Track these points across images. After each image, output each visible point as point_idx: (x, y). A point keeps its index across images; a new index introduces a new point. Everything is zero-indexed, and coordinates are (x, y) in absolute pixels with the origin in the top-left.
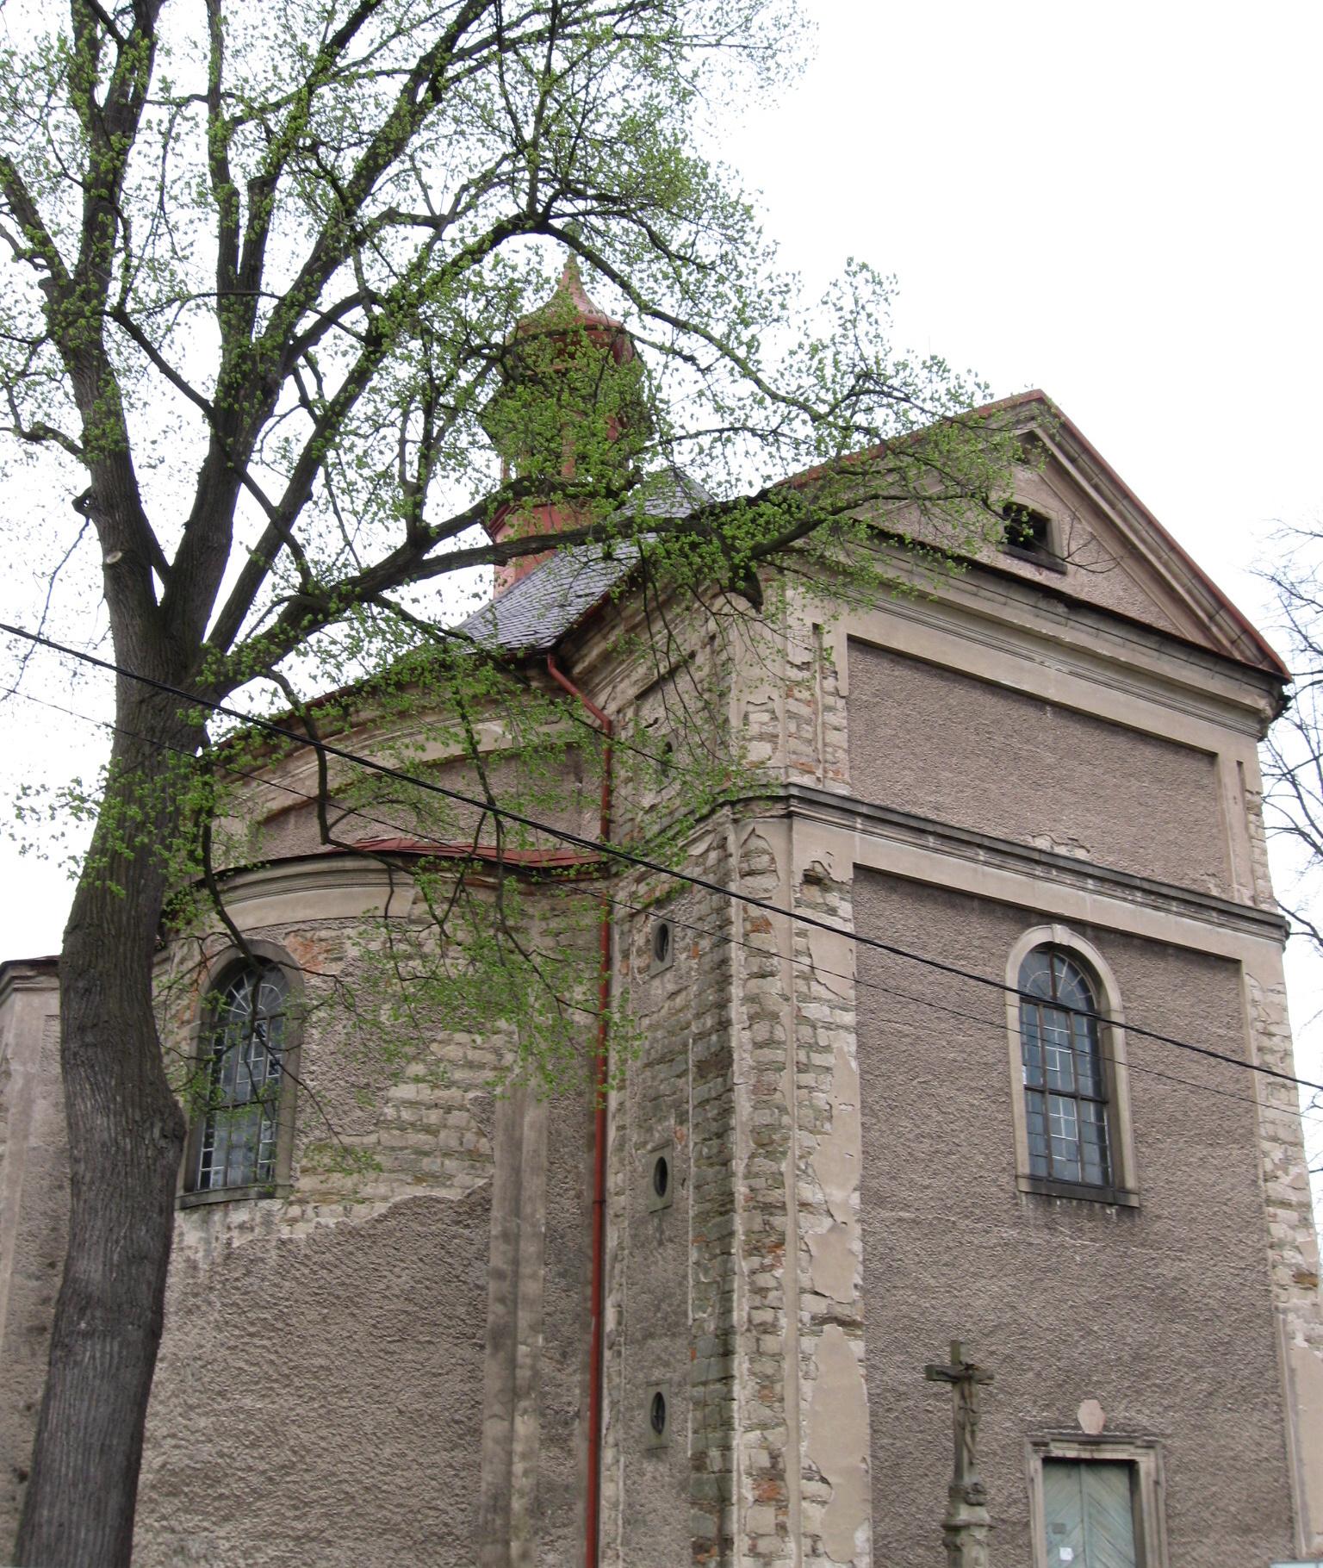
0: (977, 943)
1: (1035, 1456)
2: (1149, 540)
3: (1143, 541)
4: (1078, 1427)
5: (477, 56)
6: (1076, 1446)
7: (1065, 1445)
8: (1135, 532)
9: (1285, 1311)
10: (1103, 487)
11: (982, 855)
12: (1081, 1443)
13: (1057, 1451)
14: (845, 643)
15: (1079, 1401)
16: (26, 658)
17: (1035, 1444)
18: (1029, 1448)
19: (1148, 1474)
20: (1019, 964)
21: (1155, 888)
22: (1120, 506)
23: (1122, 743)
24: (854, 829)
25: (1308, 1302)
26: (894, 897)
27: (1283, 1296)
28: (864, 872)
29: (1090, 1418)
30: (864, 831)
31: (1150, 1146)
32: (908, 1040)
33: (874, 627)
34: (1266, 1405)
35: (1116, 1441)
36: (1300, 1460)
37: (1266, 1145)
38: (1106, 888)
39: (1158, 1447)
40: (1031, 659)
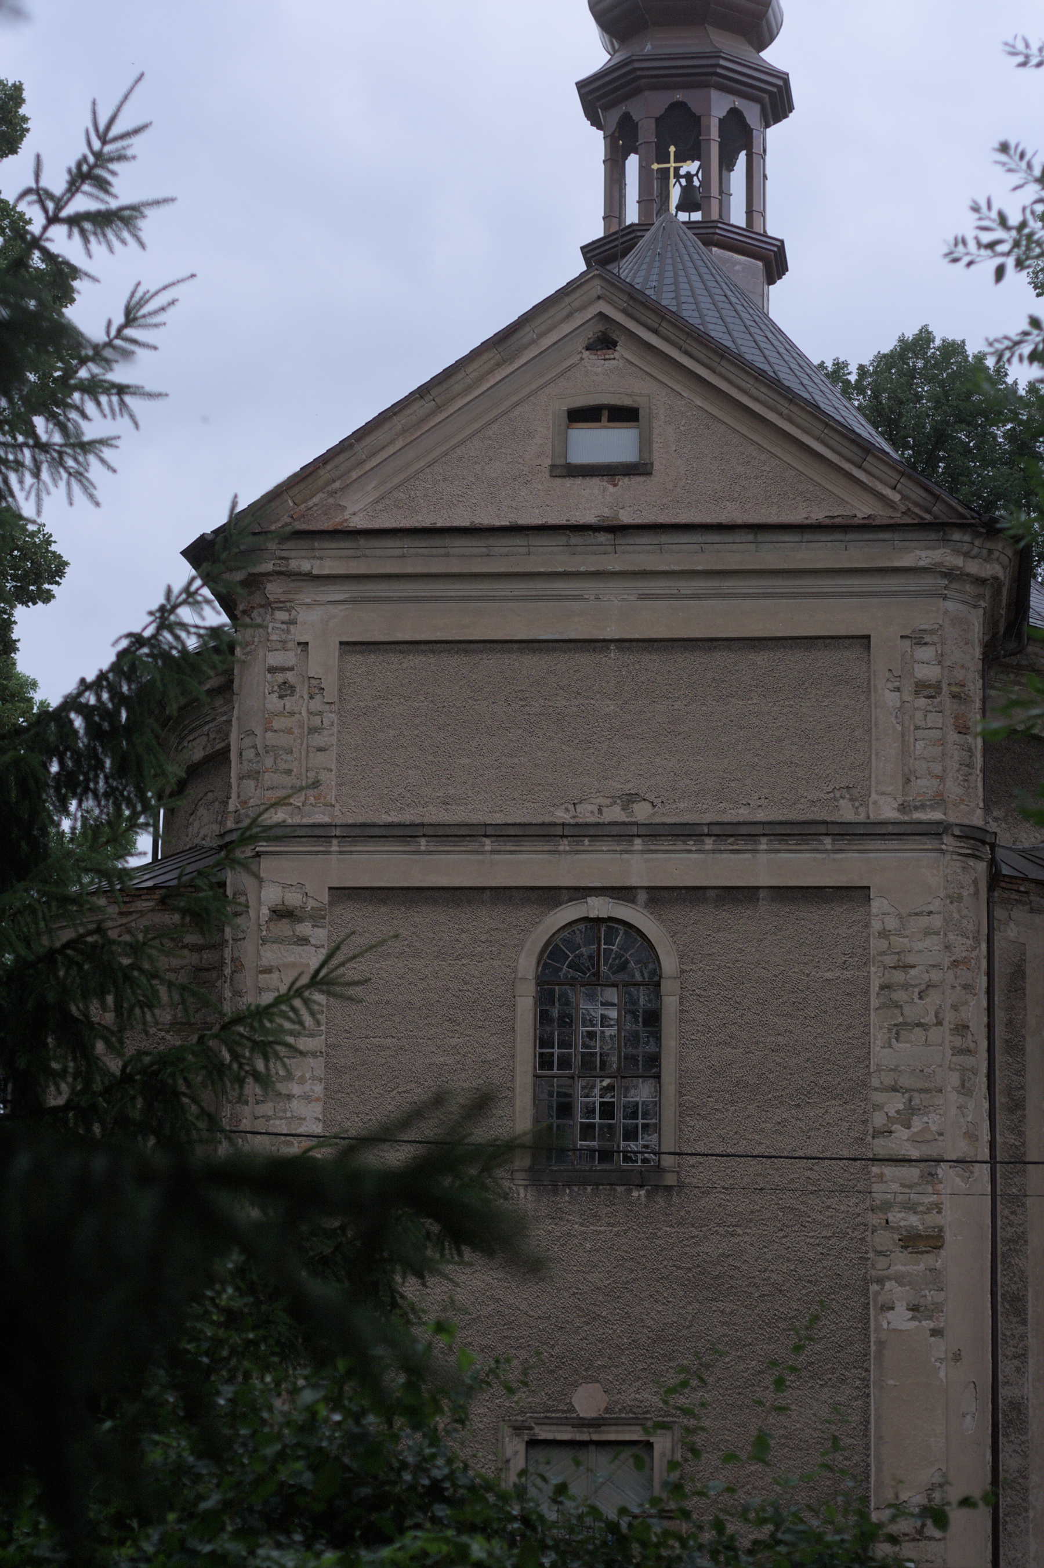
0: (484, 937)
1: (516, 1440)
2: (763, 397)
3: (756, 399)
4: (572, 1409)
5: (412, 1134)
6: (569, 1428)
7: (554, 1428)
8: (745, 392)
9: (881, 1281)
10: (695, 352)
11: (488, 844)
12: (573, 1426)
13: (544, 1433)
14: (338, 645)
15: (575, 1385)
16: (908, 780)
17: (515, 1428)
18: (507, 1430)
19: (663, 1454)
20: (538, 950)
21: (729, 830)
22: (719, 369)
23: (721, 658)
24: (329, 853)
25: (922, 1266)
26: (383, 909)
27: (881, 1263)
28: (342, 894)
29: (588, 1401)
30: (341, 853)
31: (704, 1118)
32: (388, 1052)
33: (373, 625)
34: (843, 1381)
35: (618, 1422)
36: (879, 1437)
37: (879, 1097)
38: (729, 844)
39: (676, 1427)
40: (580, 598)
